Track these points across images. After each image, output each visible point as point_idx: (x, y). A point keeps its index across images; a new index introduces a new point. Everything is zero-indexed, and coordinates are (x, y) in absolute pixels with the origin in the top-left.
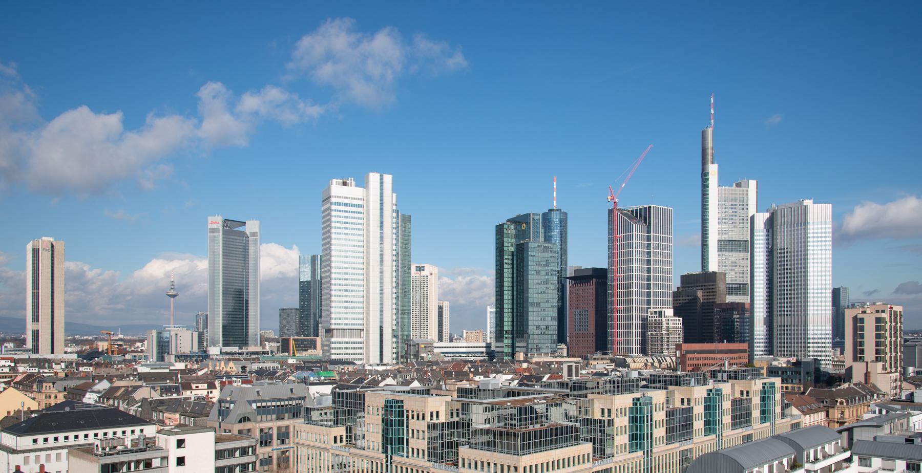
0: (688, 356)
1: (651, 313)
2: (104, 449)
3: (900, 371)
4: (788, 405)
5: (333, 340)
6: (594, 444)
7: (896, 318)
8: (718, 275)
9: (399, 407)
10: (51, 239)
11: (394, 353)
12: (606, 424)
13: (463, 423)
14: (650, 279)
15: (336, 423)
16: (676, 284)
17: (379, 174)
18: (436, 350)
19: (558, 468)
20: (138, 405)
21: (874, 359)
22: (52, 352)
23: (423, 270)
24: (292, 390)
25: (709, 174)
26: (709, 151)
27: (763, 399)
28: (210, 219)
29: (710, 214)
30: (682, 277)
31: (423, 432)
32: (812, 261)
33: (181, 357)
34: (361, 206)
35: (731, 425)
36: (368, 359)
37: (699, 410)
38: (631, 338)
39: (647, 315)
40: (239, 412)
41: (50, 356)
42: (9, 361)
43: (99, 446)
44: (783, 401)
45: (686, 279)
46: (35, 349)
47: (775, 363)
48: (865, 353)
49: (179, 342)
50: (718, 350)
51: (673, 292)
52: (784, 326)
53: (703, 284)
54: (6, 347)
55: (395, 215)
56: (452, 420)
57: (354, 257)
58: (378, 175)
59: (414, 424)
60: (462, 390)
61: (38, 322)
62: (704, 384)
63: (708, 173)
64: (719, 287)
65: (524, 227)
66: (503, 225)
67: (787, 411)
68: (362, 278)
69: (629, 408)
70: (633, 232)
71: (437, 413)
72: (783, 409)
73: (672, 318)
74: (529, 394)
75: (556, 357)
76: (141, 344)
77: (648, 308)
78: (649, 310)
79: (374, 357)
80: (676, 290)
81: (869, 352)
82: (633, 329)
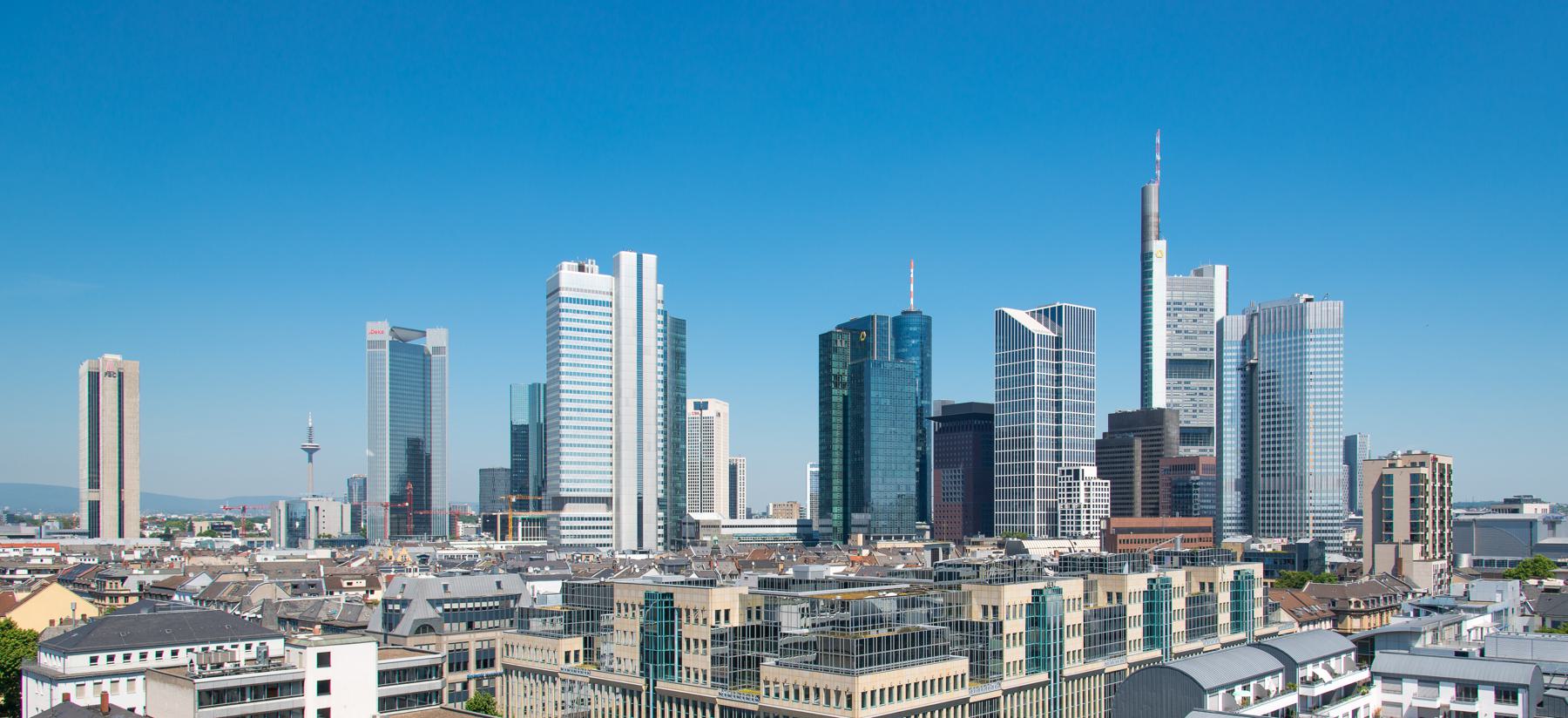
0: (1120, 537)
1: (1063, 474)
2: (202, 667)
3: (1449, 557)
4: (1275, 607)
5: (564, 514)
6: (971, 661)
7: (1442, 476)
8: (1166, 413)
9: (667, 603)
10: (119, 358)
11: (659, 527)
12: (991, 630)
13: (767, 628)
14: (1061, 444)
15: (569, 631)
16: (1100, 428)
17: (635, 254)
18: (725, 531)
19: (915, 696)
20: (256, 610)
21: (1409, 538)
22: (121, 535)
23: (706, 408)
24: (499, 584)
25: (1154, 255)
26: (1153, 220)
27: (1236, 596)
28: (370, 326)
29: (1154, 315)
30: (1111, 416)
31: (705, 642)
32: (1312, 410)
33: (322, 542)
34: (611, 304)
35: (1185, 634)
36: (619, 545)
37: (1135, 609)
38: (1031, 512)
39: (1056, 477)
40: (415, 618)
41: (118, 542)
42: (53, 549)
43: (195, 662)
44: (1266, 602)
45: (1117, 421)
46: (94, 531)
47: (1254, 546)
48: (1394, 505)
49: (321, 519)
50: (1166, 528)
51: (1097, 441)
52: (1269, 492)
53: (1144, 428)
54: (48, 527)
55: (661, 318)
56: (750, 624)
57: (593, 463)
58: (634, 255)
59: (689, 631)
60: (765, 582)
61: (98, 488)
62: (1143, 571)
63: (1152, 253)
64: (1168, 433)
65: (863, 337)
66: (830, 333)
67: (1272, 618)
68: (609, 452)
69: (1027, 605)
70: (1033, 358)
71: (727, 612)
72: (1265, 612)
73: (1095, 481)
74: (870, 585)
75: (914, 541)
76: (262, 525)
77: (1057, 465)
78: (1059, 468)
79: (629, 541)
80: (1101, 438)
81: (1401, 530)
82: (1033, 498)
